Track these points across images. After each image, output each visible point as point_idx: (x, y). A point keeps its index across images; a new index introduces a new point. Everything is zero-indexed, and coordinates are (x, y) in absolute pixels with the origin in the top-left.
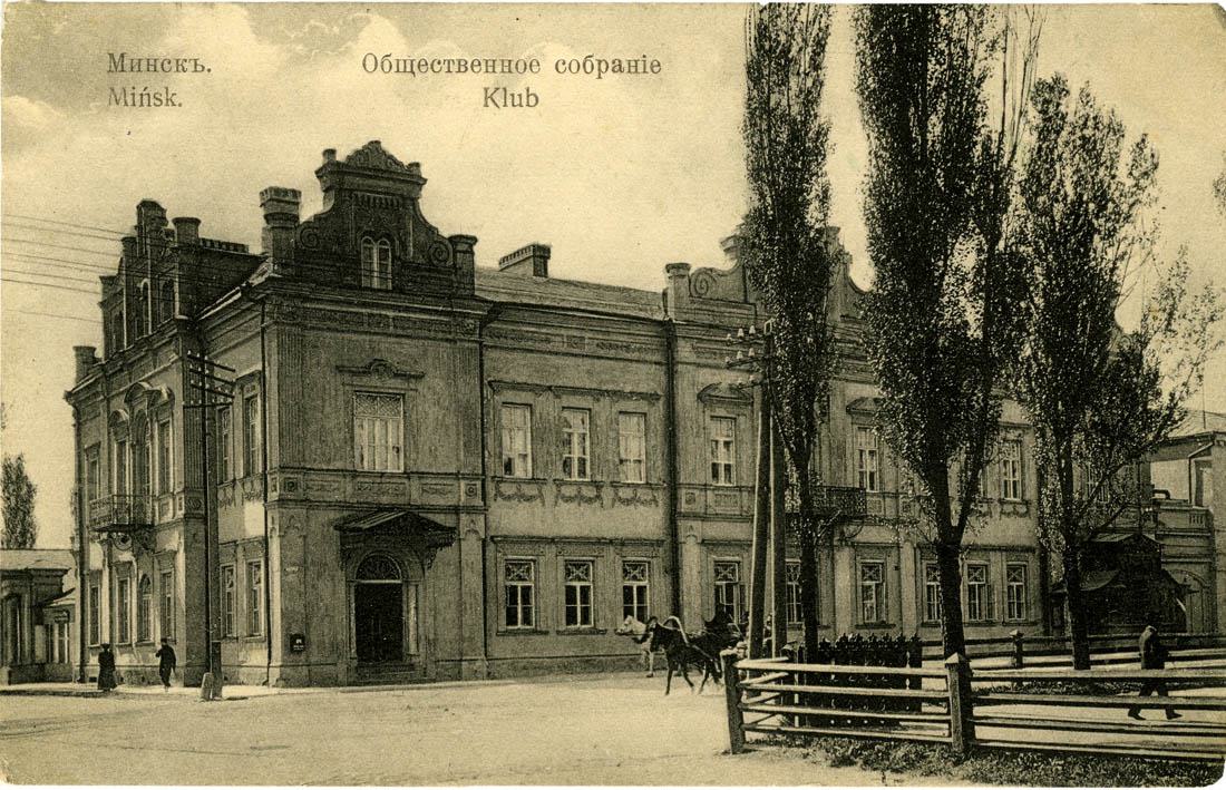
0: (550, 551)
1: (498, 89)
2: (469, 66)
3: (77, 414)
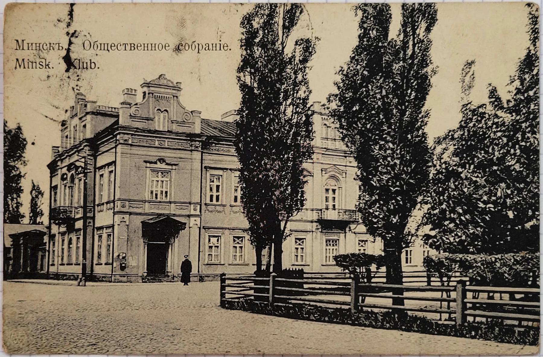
0: (227, 232)
2: (136, 47)
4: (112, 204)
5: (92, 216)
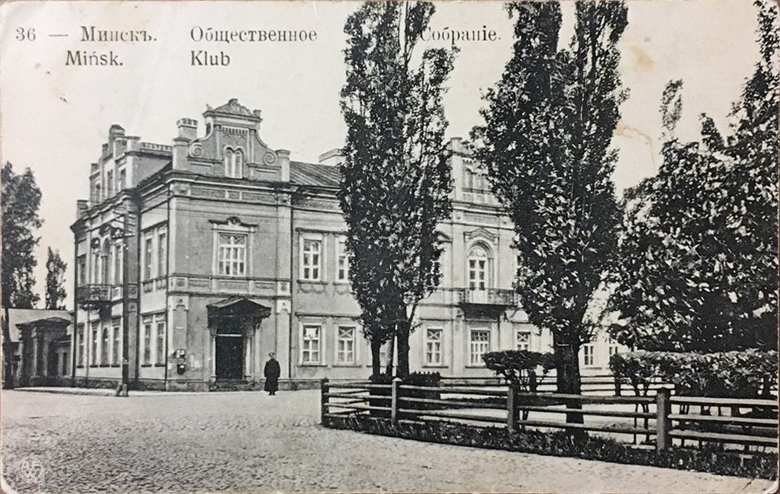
1: (201, 52)
2: (267, 36)
3: (76, 237)
4: (164, 281)
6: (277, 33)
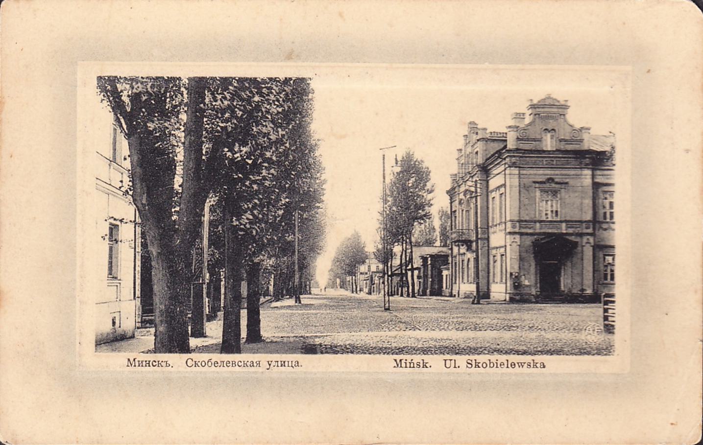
4: (504, 225)
5: (592, 232)
6: (231, 363)
